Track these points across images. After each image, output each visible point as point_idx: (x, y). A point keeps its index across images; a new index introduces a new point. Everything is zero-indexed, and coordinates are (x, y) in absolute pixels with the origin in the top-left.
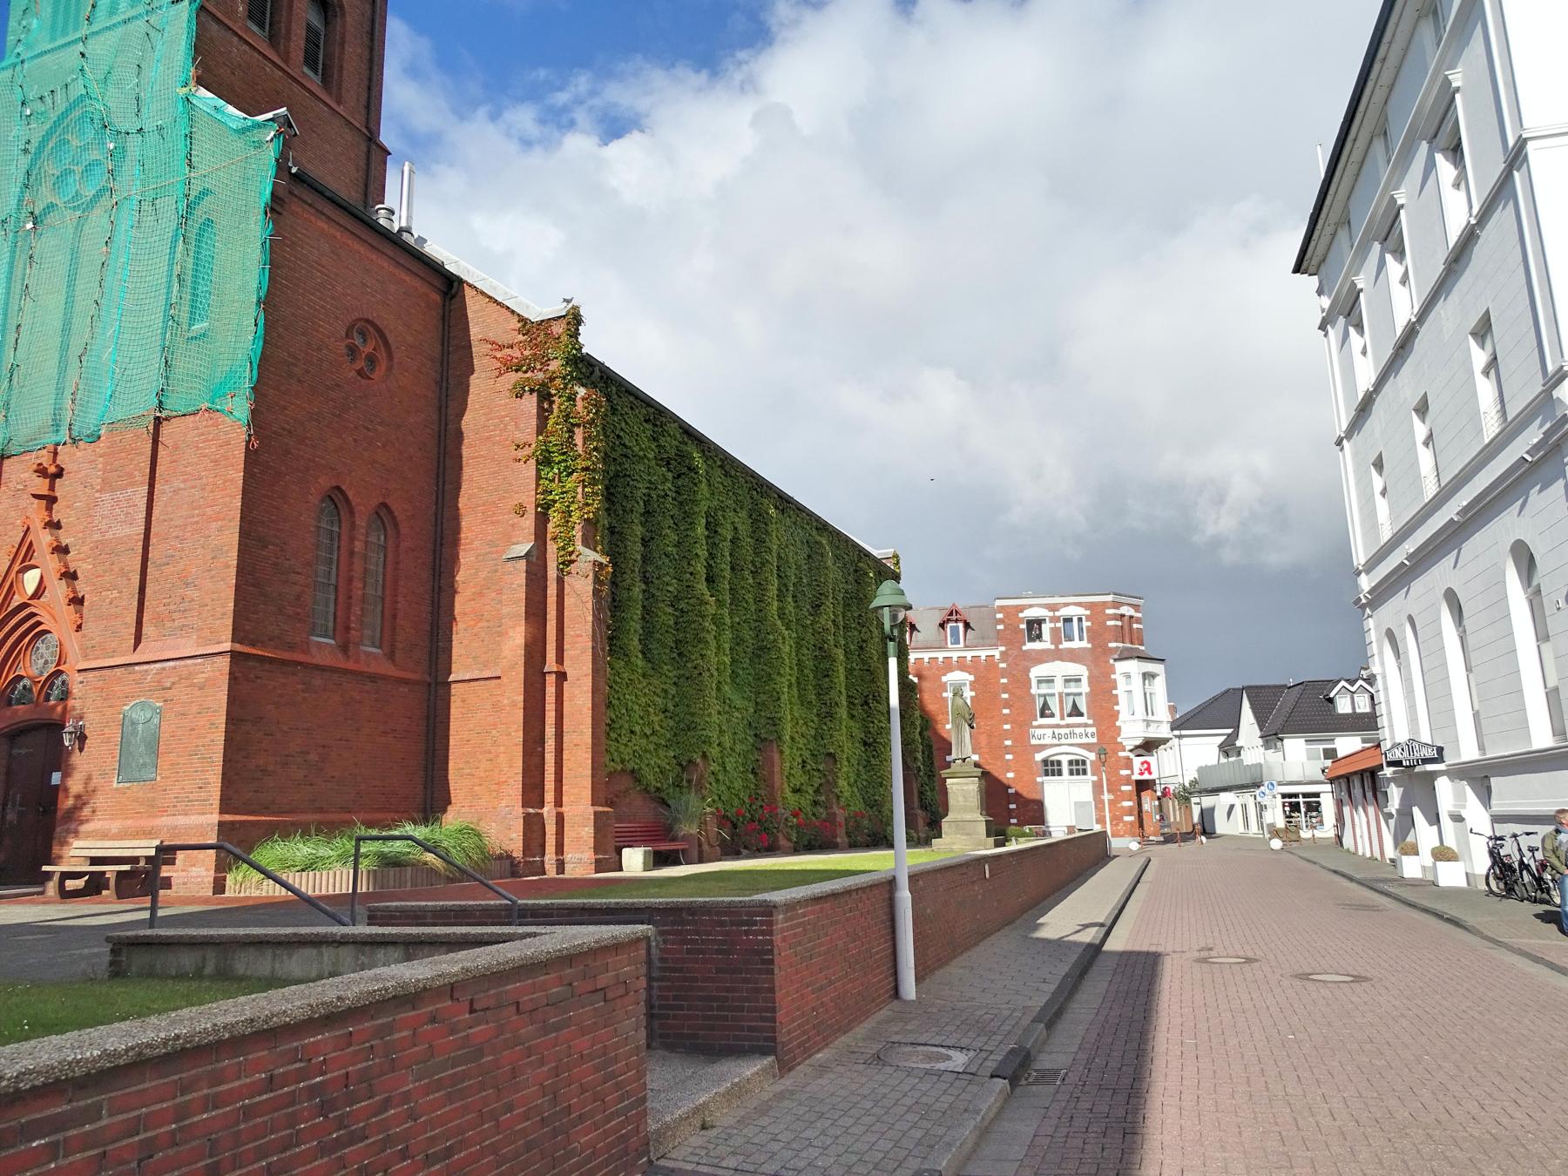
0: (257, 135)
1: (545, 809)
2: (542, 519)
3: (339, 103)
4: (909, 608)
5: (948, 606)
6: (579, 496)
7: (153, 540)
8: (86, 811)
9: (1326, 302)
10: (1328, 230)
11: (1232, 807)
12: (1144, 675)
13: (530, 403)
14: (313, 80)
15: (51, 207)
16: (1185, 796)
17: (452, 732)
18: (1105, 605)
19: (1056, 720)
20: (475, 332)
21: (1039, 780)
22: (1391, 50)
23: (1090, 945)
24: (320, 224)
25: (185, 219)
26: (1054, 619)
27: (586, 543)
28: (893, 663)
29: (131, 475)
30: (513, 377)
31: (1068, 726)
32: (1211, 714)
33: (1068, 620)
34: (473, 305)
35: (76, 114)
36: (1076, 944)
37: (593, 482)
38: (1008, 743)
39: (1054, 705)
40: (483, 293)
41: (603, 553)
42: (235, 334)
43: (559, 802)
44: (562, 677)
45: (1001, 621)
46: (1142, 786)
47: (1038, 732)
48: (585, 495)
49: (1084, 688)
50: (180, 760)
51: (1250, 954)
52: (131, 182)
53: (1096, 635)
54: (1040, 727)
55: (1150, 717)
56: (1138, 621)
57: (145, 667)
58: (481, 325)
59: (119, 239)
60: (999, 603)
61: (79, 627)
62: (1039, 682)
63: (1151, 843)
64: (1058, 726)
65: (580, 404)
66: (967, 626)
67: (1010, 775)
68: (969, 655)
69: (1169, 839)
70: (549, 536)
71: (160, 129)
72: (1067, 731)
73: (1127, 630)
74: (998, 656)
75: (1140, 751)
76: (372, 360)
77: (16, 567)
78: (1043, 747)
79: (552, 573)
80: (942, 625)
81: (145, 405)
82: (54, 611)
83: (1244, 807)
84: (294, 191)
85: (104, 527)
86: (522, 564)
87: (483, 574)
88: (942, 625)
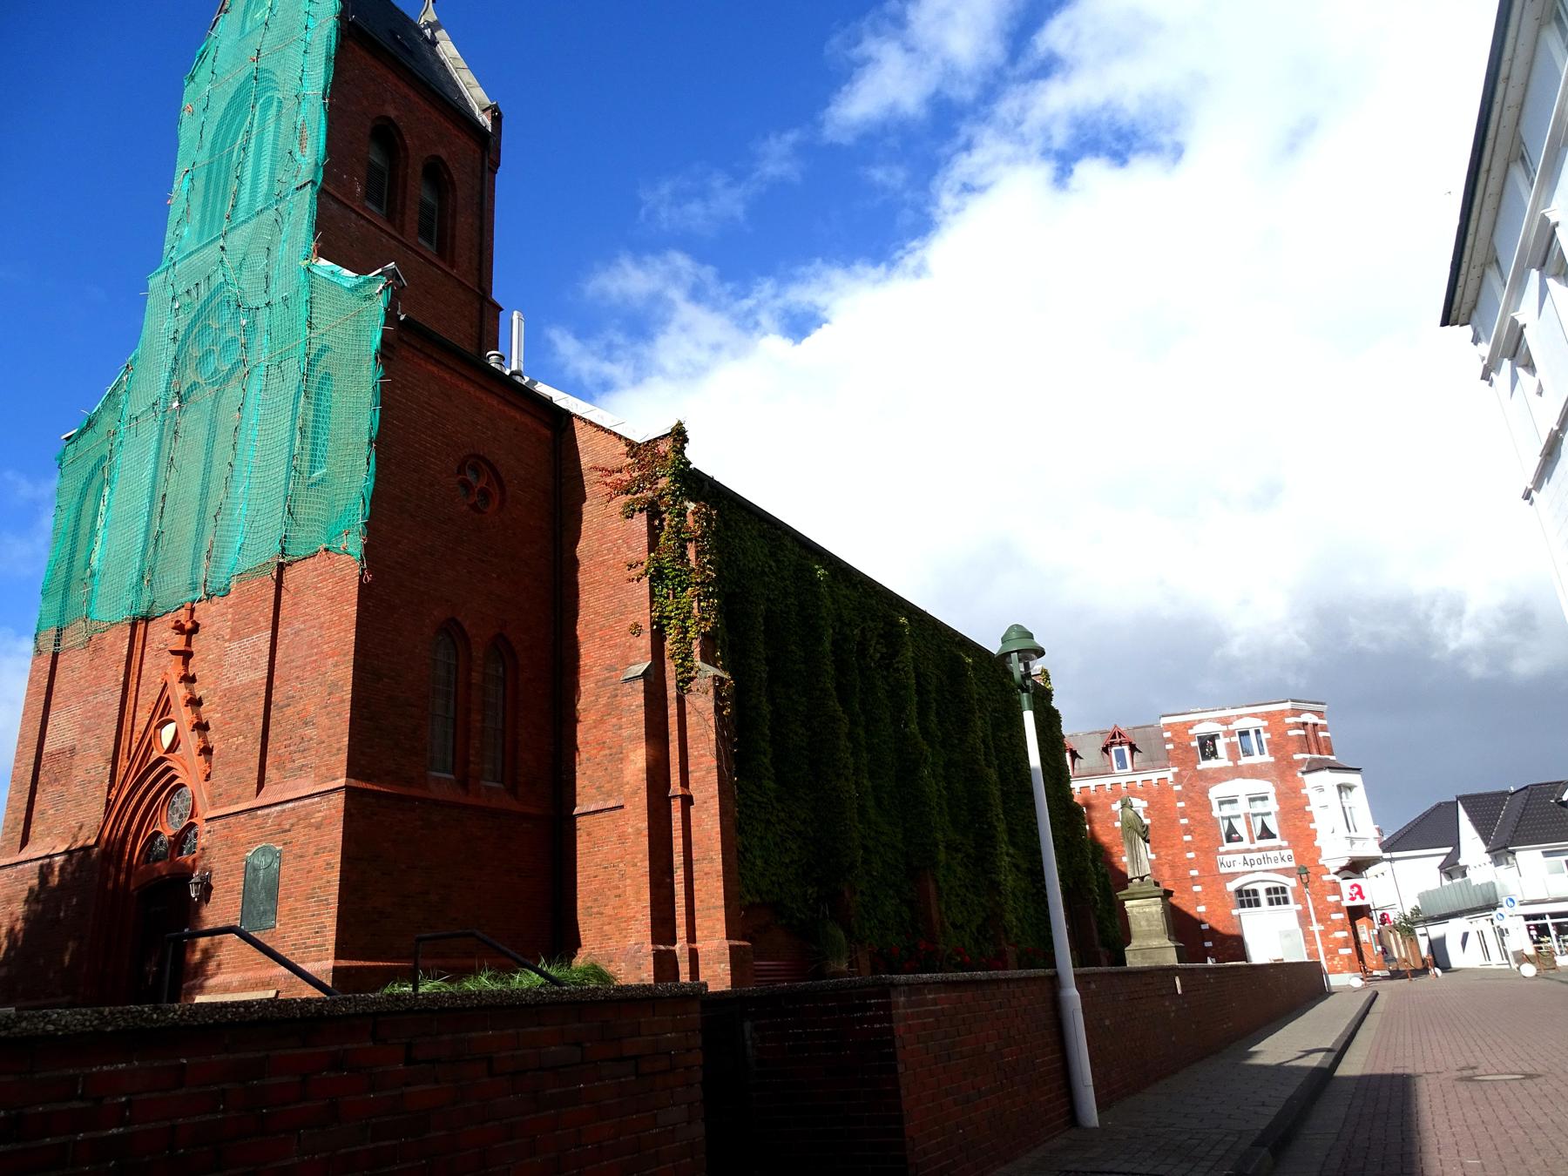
0: (368, 290)
1: (678, 946)
2: (658, 637)
3: (452, 267)
4: (1040, 653)
5: (1110, 728)
6: (695, 611)
7: (276, 683)
8: (212, 965)
9: (1485, 349)
10: (1475, 273)
11: (1466, 935)
12: (1339, 787)
13: (640, 522)
14: (429, 249)
15: (195, 385)
16: (1407, 929)
17: (579, 869)
18: (1282, 712)
19: (1245, 844)
20: (585, 461)
21: (1235, 912)
22: (1514, 68)
23: (1316, 1070)
24: (430, 367)
25: (306, 376)
26: (1229, 734)
27: (704, 659)
28: (1029, 717)
29: (256, 622)
30: (624, 499)
31: (1260, 850)
32: (1427, 831)
33: (1244, 734)
34: (582, 435)
35: (217, 300)
36: (1298, 1068)
37: (707, 596)
38: (1194, 873)
39: (1240, 826)
40: (591, 423)
41: (724, 668)
42: (351, 476)
43: (691, 937)
44: (687, 801)
45: (1169, 740)
46: (1357, 913)
47: (1227, 858)
48: (701, 609)
49: (1272, 805)
50: (298, 905)
51: (1528, 1070)
52: (262, 351)
53: (1279, 746)
54: (1228, 853)
55: (1353, 834)
56: (1324, 728)
57: (267, 811)
58: (591, 453)
59: (251, 402)
60: (1165, 720)
61: (208, 777)
62: (1221, 803)
63: (1376, 979)
64: (1248, 851)
65: (690, 519)
66: (1133, 748)
67: (1201, 909)
68: (1139, 779)
69: (1396, 975)
70: (667, 653)
71: (285, 299)
72: (1260, 855)
73: (1311, 739)
74: (1171, 779)
75: (1348, 873)
76: (485, 494)
77: (155, 723)
78: (1234, 875)
79: (672, 693)
80: (1106, 750)
81: (268, 552)
82: (187, 767)
83: (1481, 934)
84: (404, 343)
85: (231, 675)
86: (640, 685)
87: (603, 701)
88: (1106, 750)
